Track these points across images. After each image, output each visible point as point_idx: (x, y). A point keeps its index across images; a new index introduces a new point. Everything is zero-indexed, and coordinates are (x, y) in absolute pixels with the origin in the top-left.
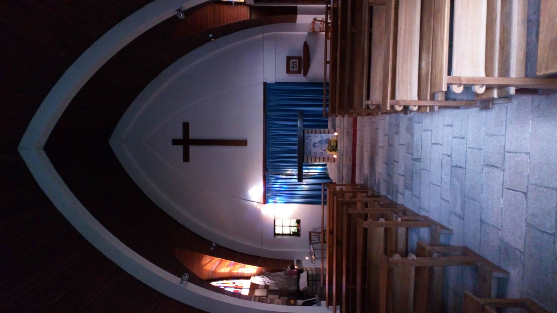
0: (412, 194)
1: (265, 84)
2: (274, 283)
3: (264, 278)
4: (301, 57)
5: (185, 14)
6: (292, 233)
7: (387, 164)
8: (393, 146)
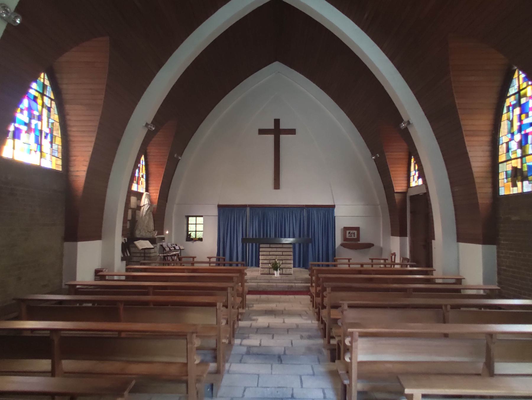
0: (243, 355)
1: (333, 207)
2: (142, 215)
3: (148, 206)
4: (359, 241)
5: (405, 128)
6: (189, 233)
7: (268, 327)
8: (288, 334)
